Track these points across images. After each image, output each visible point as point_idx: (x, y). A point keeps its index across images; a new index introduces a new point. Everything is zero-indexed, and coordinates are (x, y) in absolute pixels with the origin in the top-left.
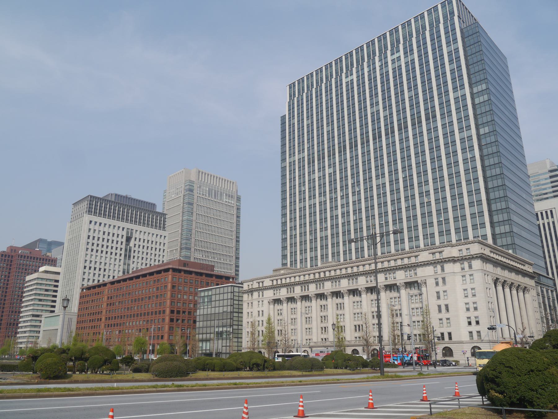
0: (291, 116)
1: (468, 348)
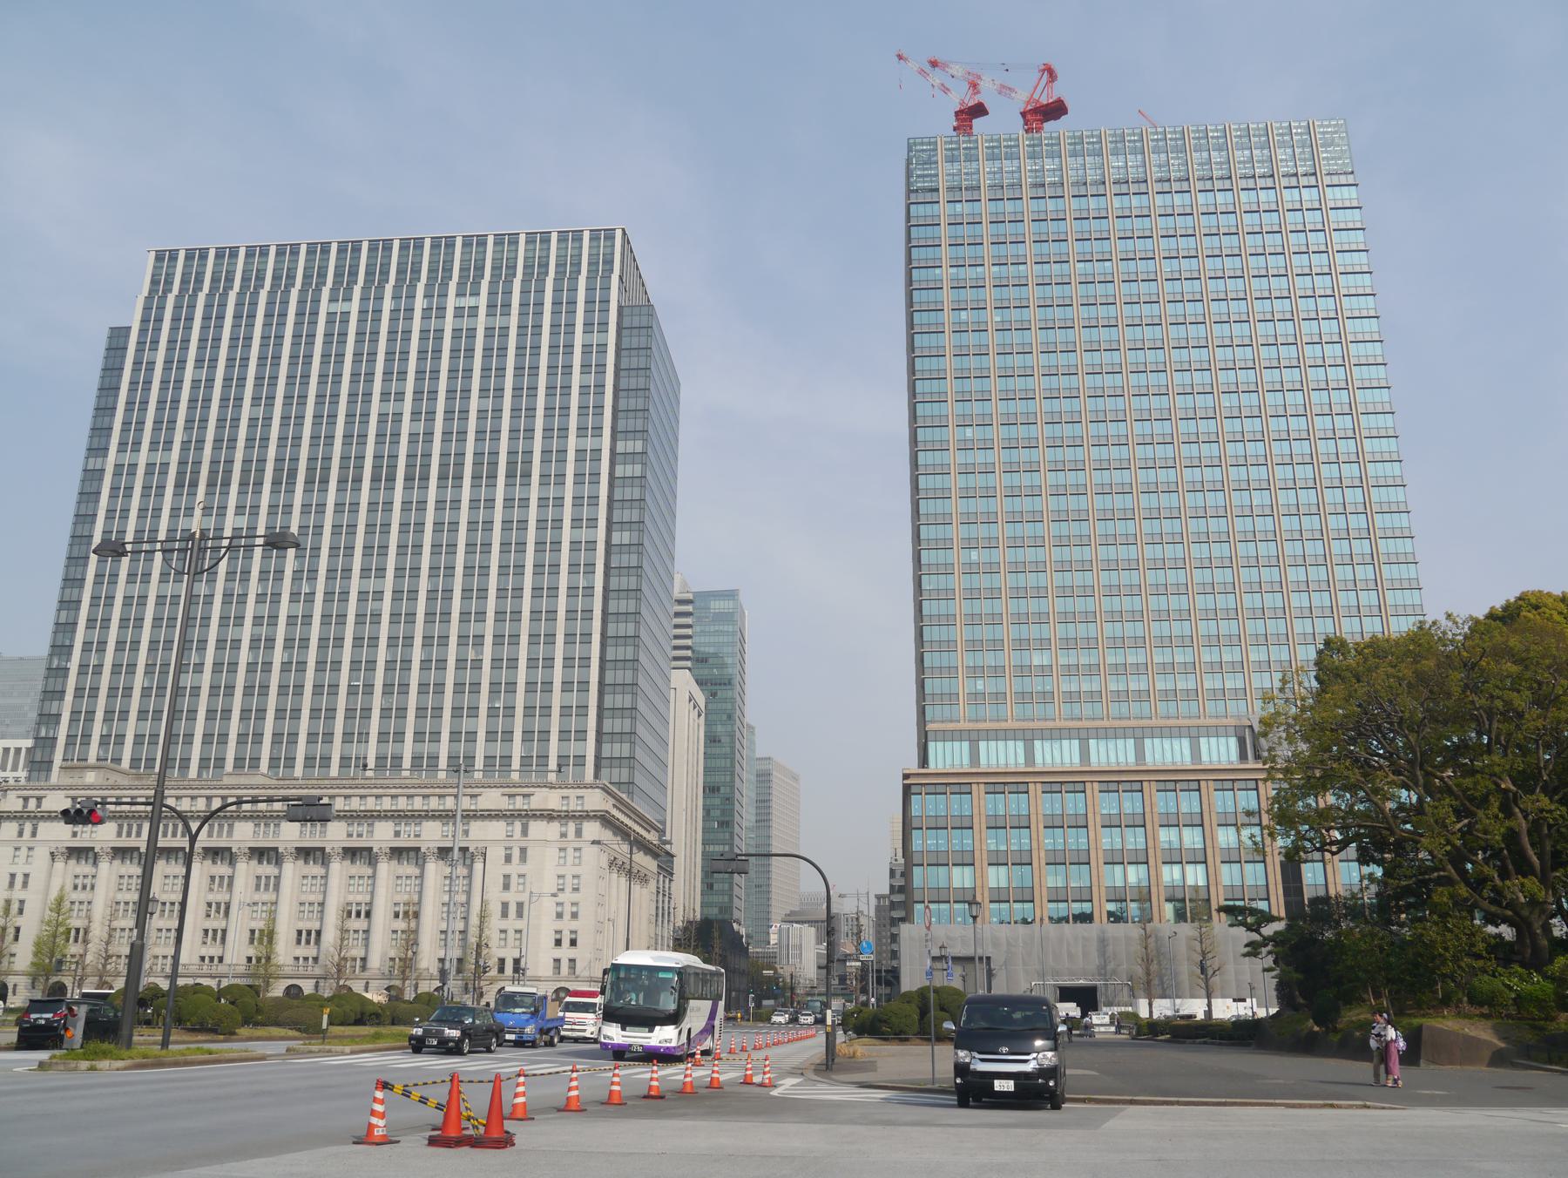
0: (149, 339)
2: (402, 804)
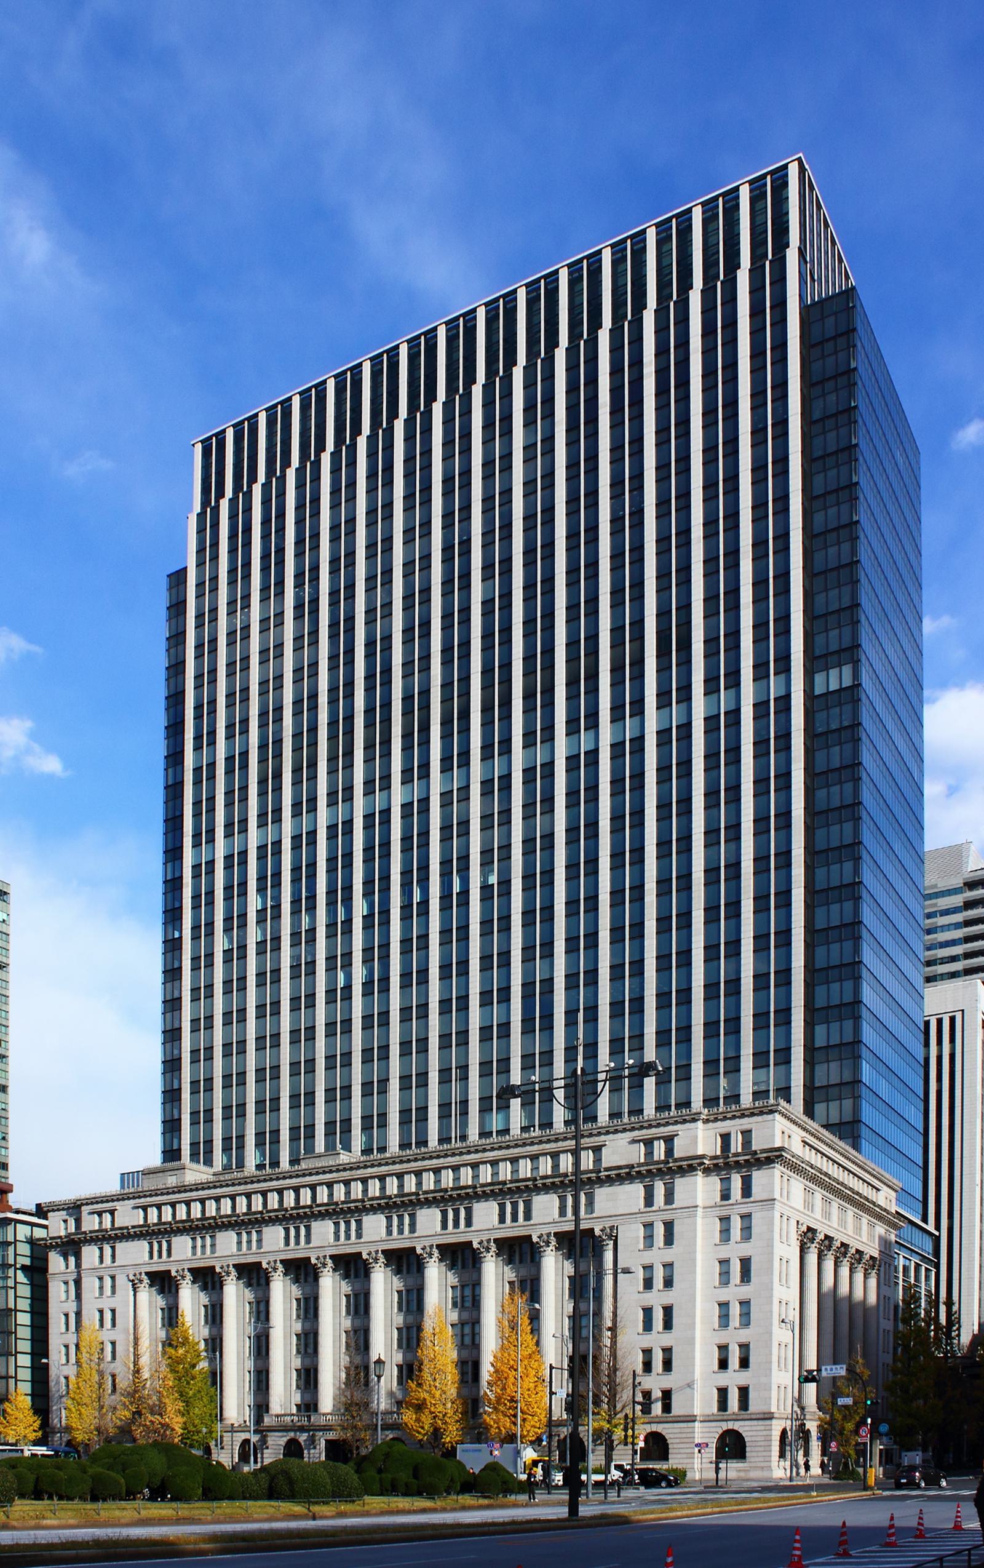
1: (706, 1434)
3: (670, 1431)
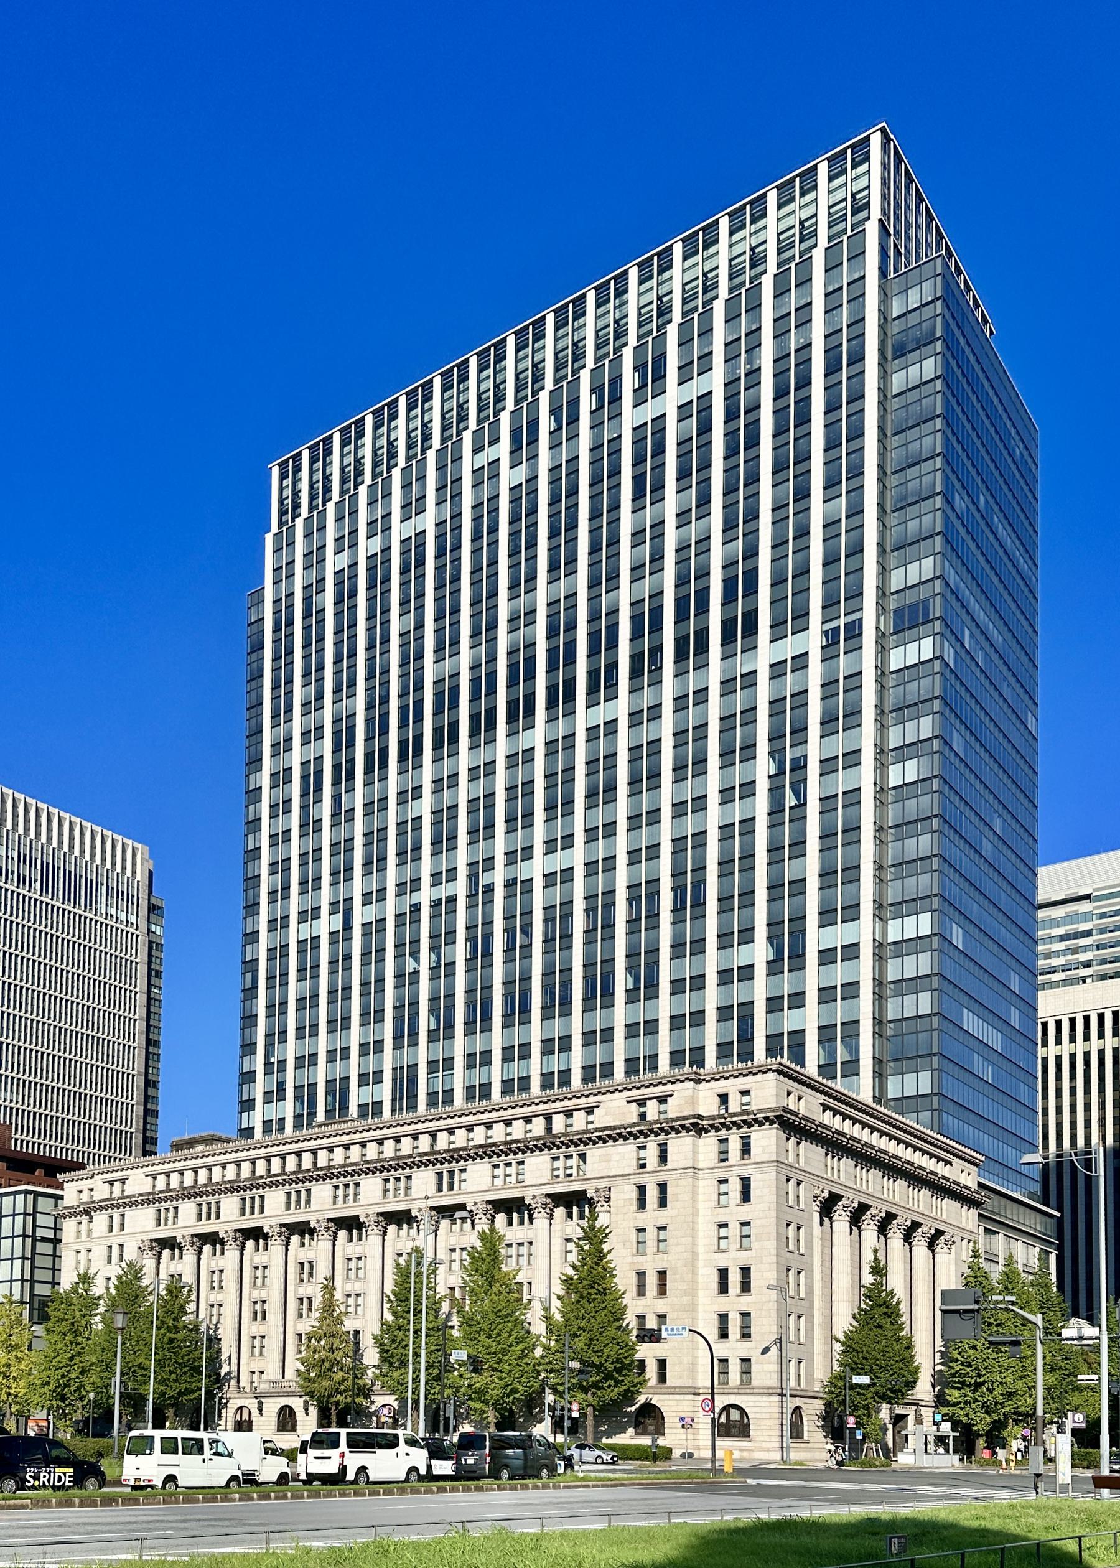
2: (498, 1133)
3: (666, 1403)
